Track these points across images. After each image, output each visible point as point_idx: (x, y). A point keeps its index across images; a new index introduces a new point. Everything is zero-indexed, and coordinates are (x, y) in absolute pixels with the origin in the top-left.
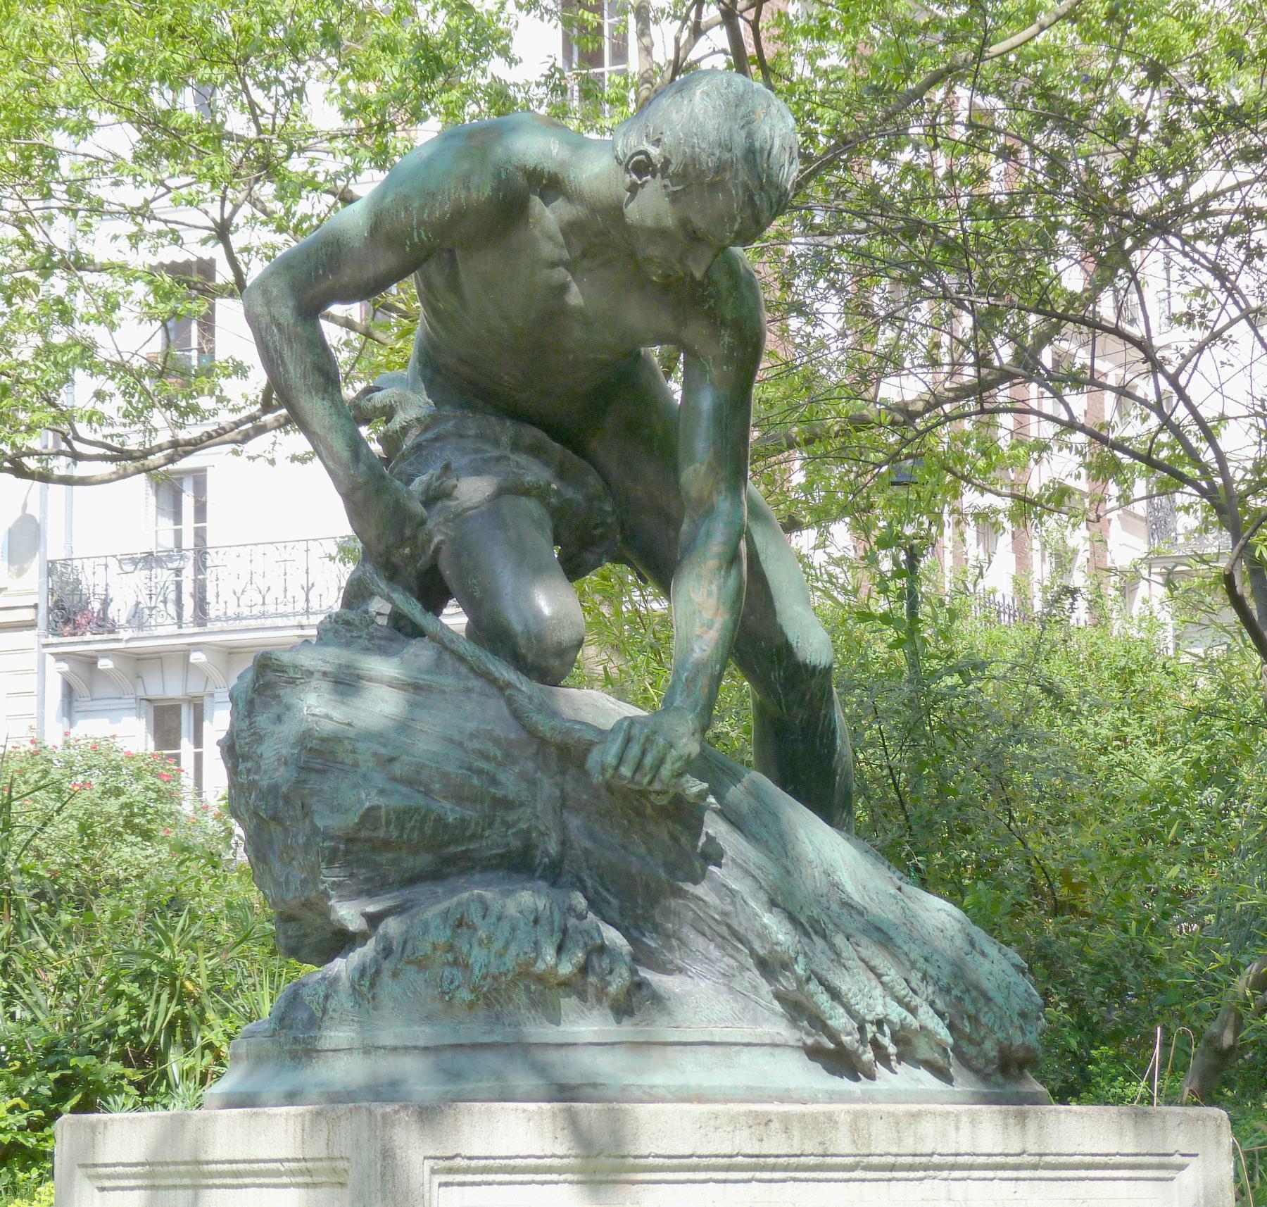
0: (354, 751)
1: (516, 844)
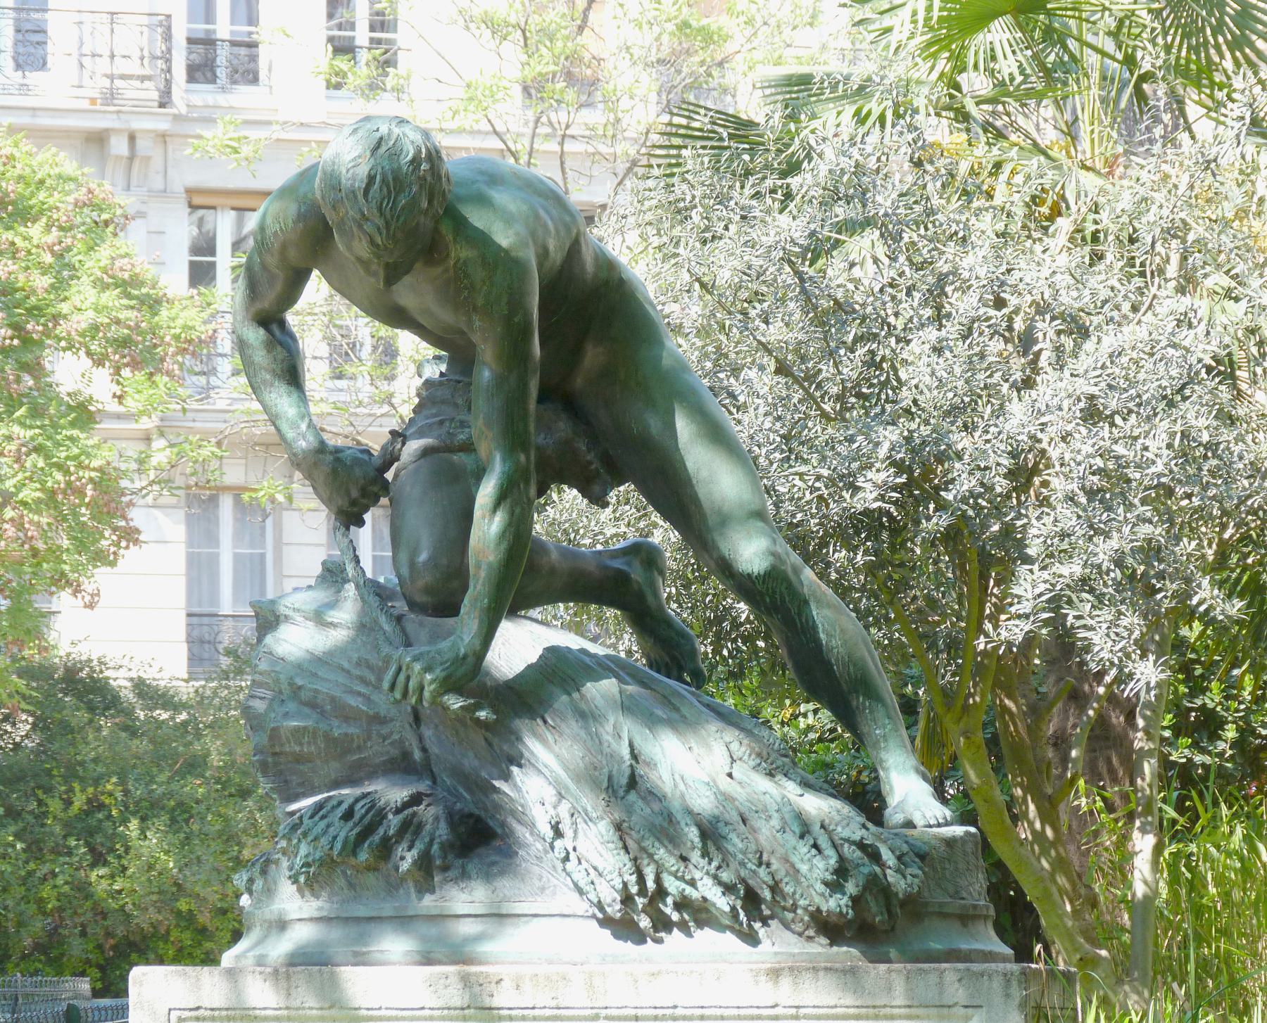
1: (395, 752)
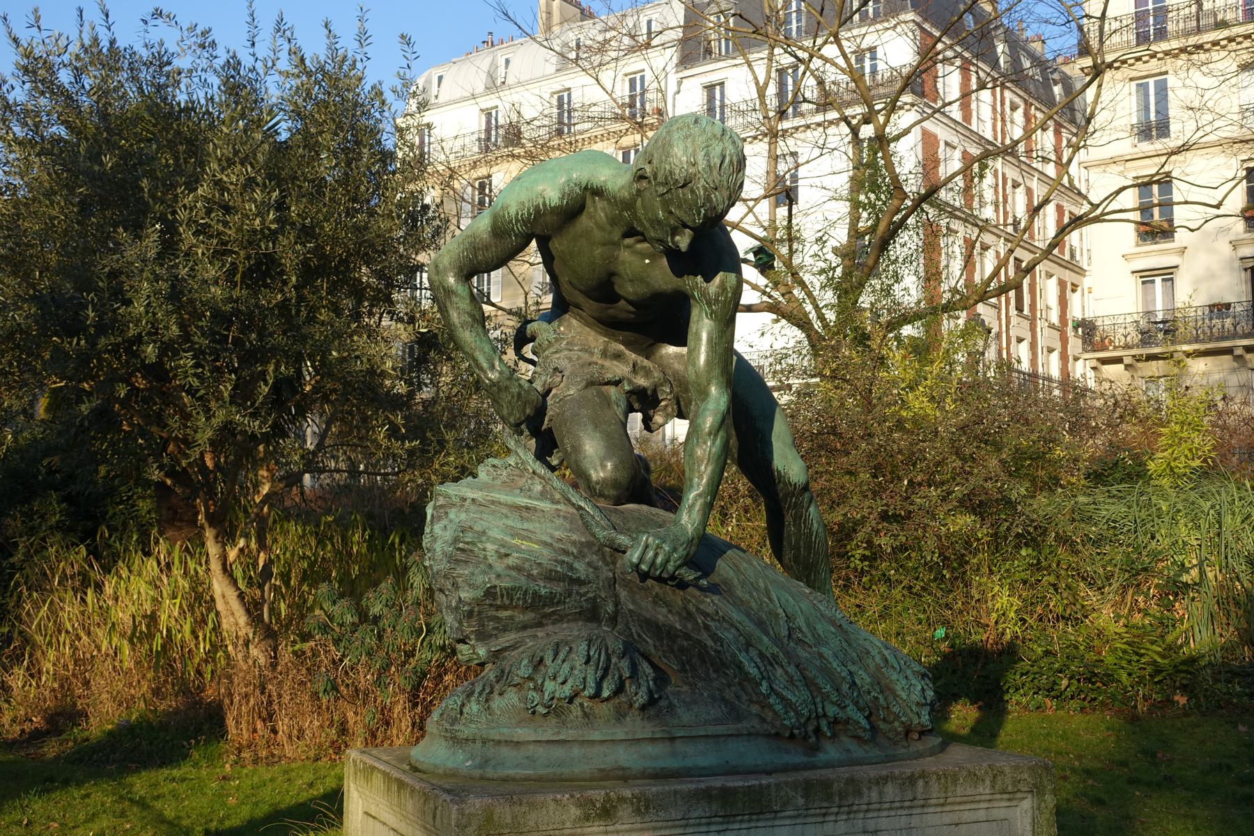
0: (484, 550)
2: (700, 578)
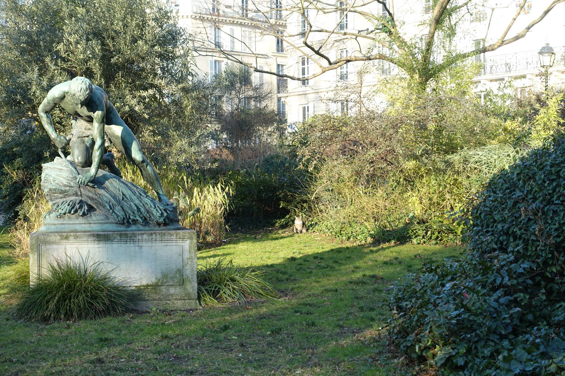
2: (184, 187)
